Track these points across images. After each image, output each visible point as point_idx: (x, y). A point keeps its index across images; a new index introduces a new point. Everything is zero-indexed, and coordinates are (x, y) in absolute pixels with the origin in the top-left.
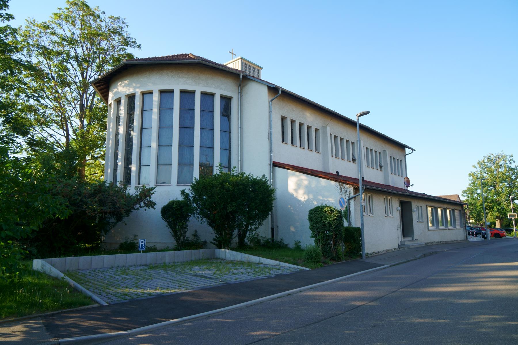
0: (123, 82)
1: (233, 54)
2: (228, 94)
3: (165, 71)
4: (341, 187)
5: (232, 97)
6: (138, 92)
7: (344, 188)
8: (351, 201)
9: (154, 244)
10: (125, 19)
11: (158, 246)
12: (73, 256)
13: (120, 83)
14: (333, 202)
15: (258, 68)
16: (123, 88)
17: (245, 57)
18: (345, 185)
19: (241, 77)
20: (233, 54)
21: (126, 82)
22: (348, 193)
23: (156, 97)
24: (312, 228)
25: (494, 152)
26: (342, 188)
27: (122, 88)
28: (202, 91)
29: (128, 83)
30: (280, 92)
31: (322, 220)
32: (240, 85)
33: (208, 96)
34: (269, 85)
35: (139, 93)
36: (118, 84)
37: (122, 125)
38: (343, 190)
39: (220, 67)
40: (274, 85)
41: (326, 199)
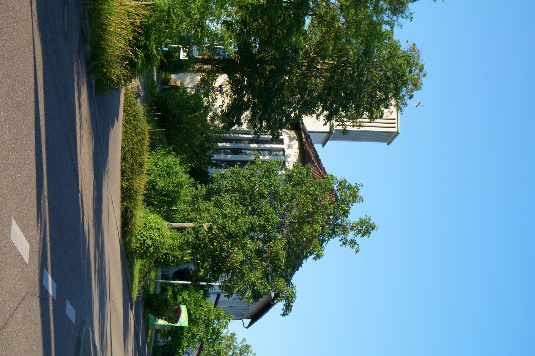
1: (419, 104)
8: (187, 354)
10: (402, 114)
18: (198, 351)
20: (419, 104)
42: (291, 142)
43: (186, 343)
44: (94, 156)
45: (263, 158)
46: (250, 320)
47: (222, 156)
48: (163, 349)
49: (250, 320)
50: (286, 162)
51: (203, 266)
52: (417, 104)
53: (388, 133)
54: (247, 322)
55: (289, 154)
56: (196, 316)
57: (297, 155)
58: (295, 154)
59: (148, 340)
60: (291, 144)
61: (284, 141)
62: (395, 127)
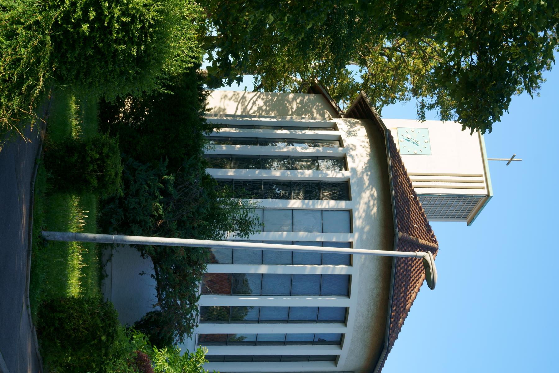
0: (376, 202)
2: (341, 362)
5: (341, 348)
6: (353, 237)
9: (109, 276)
10: (538, 94)
11: (106, 281)
13: (375, 194)
15: (470, 217)
17: (490, 204)
21: (375, 210)
25: (360, 77)
28: (346, 335)
29: (371, 216)
33: (339, 341)
35: (350, 240)
37: (303, 204)
42: (351, 127)
45: (303, 151)
47: (224, 149)
50: (347, 156)
51: (336, 8)
52: (510, 159)
53: (472, 196)
55: (353, 145)
57: (367, 145)
58: (363, 144)
60: (352, 130)
61: (339, 126)
62: (483, 188)
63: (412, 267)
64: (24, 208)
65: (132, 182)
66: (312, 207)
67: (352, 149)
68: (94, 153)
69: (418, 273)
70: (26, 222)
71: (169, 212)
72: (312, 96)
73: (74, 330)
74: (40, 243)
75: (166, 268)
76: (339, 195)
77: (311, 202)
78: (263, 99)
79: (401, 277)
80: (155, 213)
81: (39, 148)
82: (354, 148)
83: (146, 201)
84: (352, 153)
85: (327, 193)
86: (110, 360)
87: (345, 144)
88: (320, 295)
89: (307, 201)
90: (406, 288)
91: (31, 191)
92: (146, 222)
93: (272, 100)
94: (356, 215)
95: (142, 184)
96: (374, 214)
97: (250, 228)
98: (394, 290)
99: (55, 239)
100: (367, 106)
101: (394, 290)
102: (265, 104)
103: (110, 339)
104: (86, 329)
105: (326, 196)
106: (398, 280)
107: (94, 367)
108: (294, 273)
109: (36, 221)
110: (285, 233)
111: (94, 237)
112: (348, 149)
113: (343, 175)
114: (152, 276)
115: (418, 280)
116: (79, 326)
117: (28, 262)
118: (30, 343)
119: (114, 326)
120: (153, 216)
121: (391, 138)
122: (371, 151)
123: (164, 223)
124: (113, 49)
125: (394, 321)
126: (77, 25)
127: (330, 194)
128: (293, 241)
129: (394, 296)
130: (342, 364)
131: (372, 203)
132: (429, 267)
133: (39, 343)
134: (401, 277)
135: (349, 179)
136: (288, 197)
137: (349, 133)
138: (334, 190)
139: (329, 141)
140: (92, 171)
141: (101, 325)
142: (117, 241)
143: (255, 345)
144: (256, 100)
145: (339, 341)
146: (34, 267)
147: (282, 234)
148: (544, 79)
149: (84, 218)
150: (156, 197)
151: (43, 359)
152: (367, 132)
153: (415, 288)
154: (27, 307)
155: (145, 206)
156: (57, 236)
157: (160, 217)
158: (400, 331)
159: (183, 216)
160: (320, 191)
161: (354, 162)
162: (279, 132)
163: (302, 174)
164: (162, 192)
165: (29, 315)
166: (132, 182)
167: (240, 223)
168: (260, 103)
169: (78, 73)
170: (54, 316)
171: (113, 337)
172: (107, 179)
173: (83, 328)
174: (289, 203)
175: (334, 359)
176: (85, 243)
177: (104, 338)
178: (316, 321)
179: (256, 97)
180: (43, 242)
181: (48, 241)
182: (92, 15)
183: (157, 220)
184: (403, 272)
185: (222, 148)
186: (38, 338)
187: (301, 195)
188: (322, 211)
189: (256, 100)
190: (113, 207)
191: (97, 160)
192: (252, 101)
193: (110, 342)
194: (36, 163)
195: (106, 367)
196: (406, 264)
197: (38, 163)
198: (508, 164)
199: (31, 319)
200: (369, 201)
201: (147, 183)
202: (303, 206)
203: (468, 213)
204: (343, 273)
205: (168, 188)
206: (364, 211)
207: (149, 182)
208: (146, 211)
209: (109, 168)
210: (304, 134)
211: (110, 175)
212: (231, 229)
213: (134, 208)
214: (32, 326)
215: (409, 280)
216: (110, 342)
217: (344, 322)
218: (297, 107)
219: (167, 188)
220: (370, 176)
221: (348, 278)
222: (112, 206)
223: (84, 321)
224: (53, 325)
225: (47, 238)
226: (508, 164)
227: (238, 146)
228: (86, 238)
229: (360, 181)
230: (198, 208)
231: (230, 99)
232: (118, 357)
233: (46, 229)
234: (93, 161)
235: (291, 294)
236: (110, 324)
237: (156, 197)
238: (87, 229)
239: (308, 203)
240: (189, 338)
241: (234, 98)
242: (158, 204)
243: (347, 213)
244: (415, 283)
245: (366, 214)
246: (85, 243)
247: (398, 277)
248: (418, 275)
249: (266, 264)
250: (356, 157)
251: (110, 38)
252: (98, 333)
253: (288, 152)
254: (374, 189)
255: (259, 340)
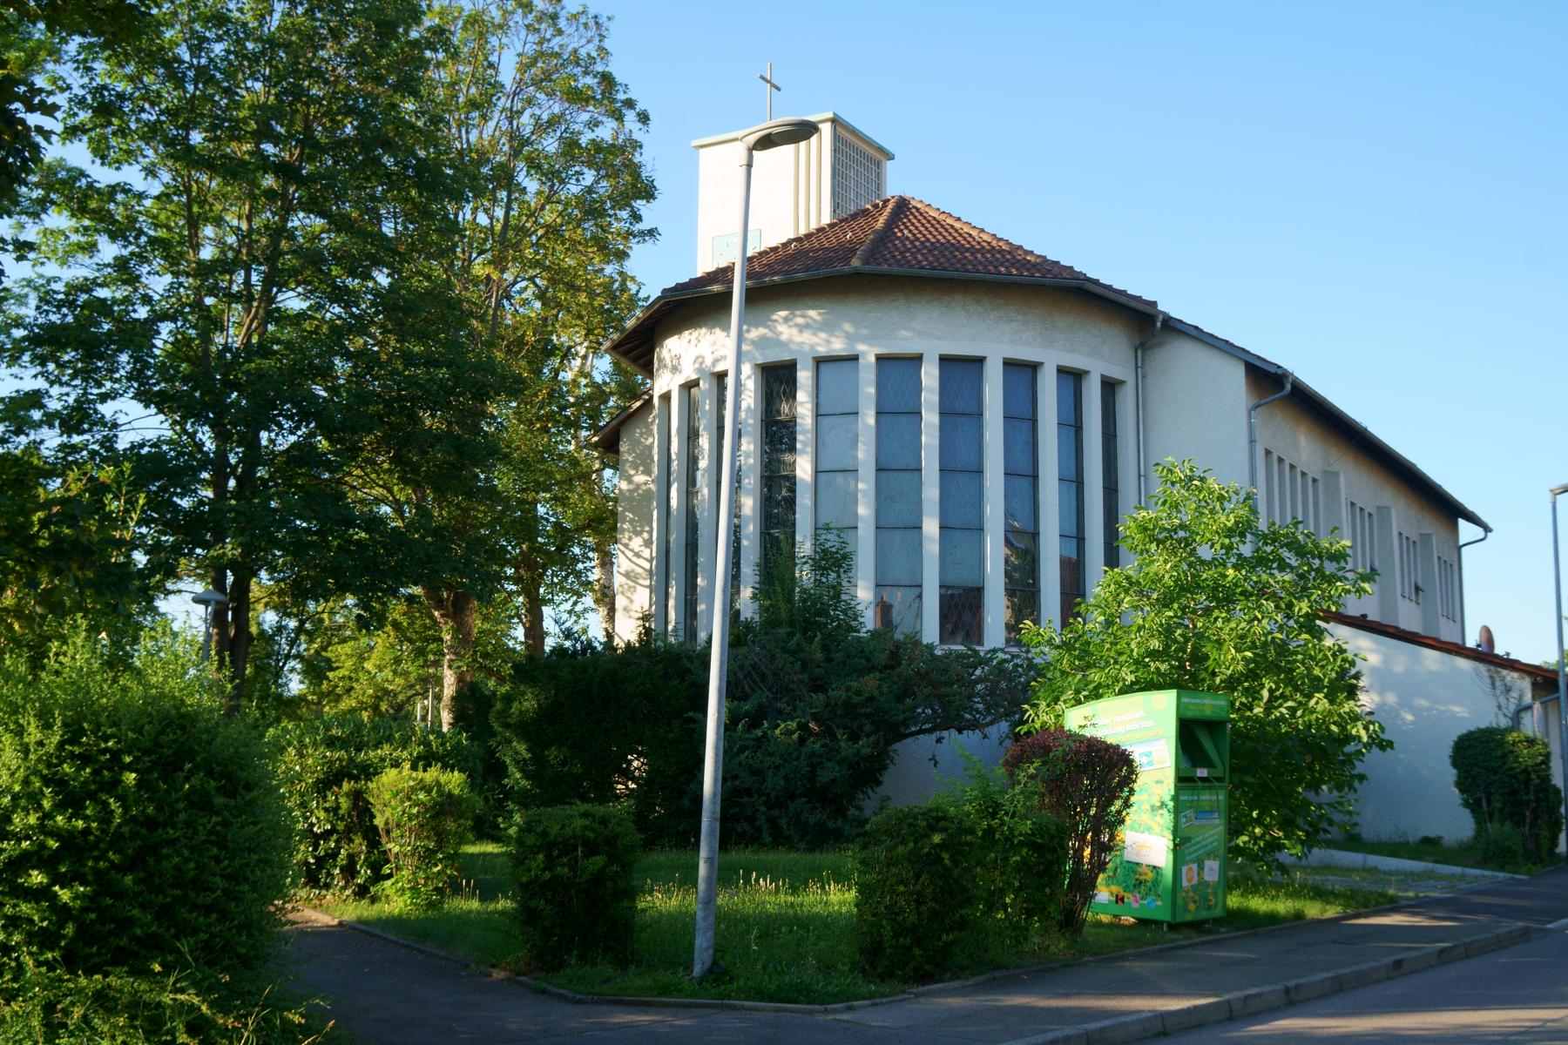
0: (798, 313)
1: (773, 86)
2: (1115, 372)
3: (959, 297)
4: (1491, 677)
5: (1087, 372)
7: (1503, 679)
8: (1523, 714)
10: (609, 19)
12: (802, 846)
13: (783, 313)
14: (1466, 715)
15: (878, 156)
16: (801, 331)
18: (1505, 672)
19: (1159, 324)
20: (773, 86)
21: (812, 313)
22: (1514, 694)
23: (930, 375)
24: (1461, 784)
26: (1497, 679)
27: (795, 331)
30: (1288, 387)
31: (1504, 763)
32: (1142, 345)
33: (1072, 378)
34: (1251, 360)
35: (872, 359)
36: (774, 312)
37: (803, 452)
38: (1498, 683)
39: (1123, 300)
40: (1279, 367)
41: (1443, 708)
42: (665, 366)
43: (1312, 703)
44: (1124, 994)
46: (1462, 523)
48: (1491, 819)
49: (1462, 523)
54: (1466, 530)
56: (1153, 654)
58: (694, 342)
59: (1332, 911)
61: (664, 390)
63: (928, 240)
64: (616, 1020)
65: (737, 782)
66: (810, 436)
67: (701, 364)
68: (534, 865)
69: (941, 230)
70: (646, 1013)
71: (795, 709)
72: (624, 447)
73: (919, 903)
74: (715, 981)
75: (904, 712)
76: (788, 384)
77: (799, 437)
78: (630, 539)
79: (942, 260)
80: (795, 736)
81: (521, 984)
82: (699, 359)
83: (771, 754)
84: (708, 362)
85: (785, 408)
86: (1003, 823)
87: (694, 377)
88: (981, 415)
89: (799, 446)
90: (968, 250)
91: (593, 1002)
92: (813, 754)
93: (631, 521)
94: (822, 350)
95: (740, 764)
96: (820, 314)
97: (834, 550)
98: (967, 271)
99: (708, 948)
100: (626, 338)
101: (967, 271)
102: (638, 534)
103: (942, 824)
104: (918, 876)
105: (790, 409)
106: (946, 265)
107: (1018, 858)
108: (937, 466)
109: (665, 990)
110: (861, 486)
111: (706, 862)
112: (700, 370)
113: (749, 377)
114: (939, 741)
115: (956, 231)
116: (912, 894)
117: (747, 1009)
118: (940, 1000)
119: (915, 817)
120: (802, 740)
121: (679, 288)
122: (705, 325)
123: (816, 717)
124: (125, 830)
125: (1028, 270)
126: (62, 913)
127: (787, 402)
128: (877, 470)
129: (978, 271)
130: (1120, 369)
131: (800, 320)
132: (769, 135)
133: (950, 980)
134: (942, 260)
135: (757, 365)
136: (792, 480)
137: (675, 369)
138: (778, 393)
139: (690, 408)
140: (572, 868)
141: (911, 845)
142: (714, 813)
143: (1084, 539)
144: (632, 550)
145: (1072, 378)
146: (762, 995)
147: (863, 491)
148: (581, 10)
149: (757, 881)
150: (765, 735)
151: (999, 967)
152: (672, 335)
153: (970, 235)
154: (849, 1009)
155: (781, 757)
156: (702, 943)
157: (803, 727)
158: (1058, 263)
159: (801, 681)
160: (781, 422)
161: (724, 358)
162: (674, 503)
163: (748, 456)
164: (755, 723)
165: (874, 1005)
166: (737, 782)
167: (825, 569)
168: (636, 543)
169: (195, 907)
170: (890, 947)
171: (938, 819)
172: (592, 835)
173: (914, 885)
174: (803, 480)
175: (1110, 387)
176: (724, 876)
177: (937, 838)
178: (1034, 421)
179: (627, 552)
180: (717, 974)
181: (715, 963)
182: (37, 878)
183: (810, 732)
184: (933, 256)
185: (702, 612)
186: (942, 981)
187: (787, 457)
188: (818, 415)
189: (632, 550)
190: (785, 820)
191: (549, 857)
192: (635, 559)
193: (948, 824)
194: (544, 992)
195: (1016, 833)
196: (919, 251)
197: (544, 985)
198: (779, 89)
199: (885, 1000)
200: (797, 325)
201: (738, 754)
202: (807, 453)
203: (870, 159)
204: (936, 371)
205: (746, 711)
206: (815, 334)
207: (735, 749)
208: (790, 754)
209: (568, 831)
210: (677, 455)
211: (585, 828)
212: (836, 592)
213: (786, 778)
214: (903, 997)
215: (953, 245)
216: (948, 824)
217: (1033, 368)
218: (643, 472)
219: (747, 714)
220: (749, 326)
221: (948, 362)
222: (783, 822)
223: (901, 882)
224: (909, 949)
225: (708, 964)
226: (779, 89)
227: (699, 580)
228: (709, 880)
229: (761, 343)
230: (788, 652)
231: (631, 601)
232: (997, 806)
233: (688, 967)
234: (550, 865)
235: (979, 472)
236: (911, 825)
237: (765, 735)
238: (689, 879)
239: (802, 442)
240: (586, 615)
241: (629, 594)
242: (778, 732)
243: (824, 367)
244: (960, 235)
245: (821, 330)
246: (724, 876)
247: (941, 264)
248: (946, 230)
249: (921, 522)
250: (717, 354)
251: (96, 837)
252: (926, 850)
253: (709, 486)
254: (775, 317)
255: (1074, 532)
